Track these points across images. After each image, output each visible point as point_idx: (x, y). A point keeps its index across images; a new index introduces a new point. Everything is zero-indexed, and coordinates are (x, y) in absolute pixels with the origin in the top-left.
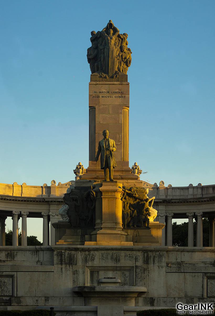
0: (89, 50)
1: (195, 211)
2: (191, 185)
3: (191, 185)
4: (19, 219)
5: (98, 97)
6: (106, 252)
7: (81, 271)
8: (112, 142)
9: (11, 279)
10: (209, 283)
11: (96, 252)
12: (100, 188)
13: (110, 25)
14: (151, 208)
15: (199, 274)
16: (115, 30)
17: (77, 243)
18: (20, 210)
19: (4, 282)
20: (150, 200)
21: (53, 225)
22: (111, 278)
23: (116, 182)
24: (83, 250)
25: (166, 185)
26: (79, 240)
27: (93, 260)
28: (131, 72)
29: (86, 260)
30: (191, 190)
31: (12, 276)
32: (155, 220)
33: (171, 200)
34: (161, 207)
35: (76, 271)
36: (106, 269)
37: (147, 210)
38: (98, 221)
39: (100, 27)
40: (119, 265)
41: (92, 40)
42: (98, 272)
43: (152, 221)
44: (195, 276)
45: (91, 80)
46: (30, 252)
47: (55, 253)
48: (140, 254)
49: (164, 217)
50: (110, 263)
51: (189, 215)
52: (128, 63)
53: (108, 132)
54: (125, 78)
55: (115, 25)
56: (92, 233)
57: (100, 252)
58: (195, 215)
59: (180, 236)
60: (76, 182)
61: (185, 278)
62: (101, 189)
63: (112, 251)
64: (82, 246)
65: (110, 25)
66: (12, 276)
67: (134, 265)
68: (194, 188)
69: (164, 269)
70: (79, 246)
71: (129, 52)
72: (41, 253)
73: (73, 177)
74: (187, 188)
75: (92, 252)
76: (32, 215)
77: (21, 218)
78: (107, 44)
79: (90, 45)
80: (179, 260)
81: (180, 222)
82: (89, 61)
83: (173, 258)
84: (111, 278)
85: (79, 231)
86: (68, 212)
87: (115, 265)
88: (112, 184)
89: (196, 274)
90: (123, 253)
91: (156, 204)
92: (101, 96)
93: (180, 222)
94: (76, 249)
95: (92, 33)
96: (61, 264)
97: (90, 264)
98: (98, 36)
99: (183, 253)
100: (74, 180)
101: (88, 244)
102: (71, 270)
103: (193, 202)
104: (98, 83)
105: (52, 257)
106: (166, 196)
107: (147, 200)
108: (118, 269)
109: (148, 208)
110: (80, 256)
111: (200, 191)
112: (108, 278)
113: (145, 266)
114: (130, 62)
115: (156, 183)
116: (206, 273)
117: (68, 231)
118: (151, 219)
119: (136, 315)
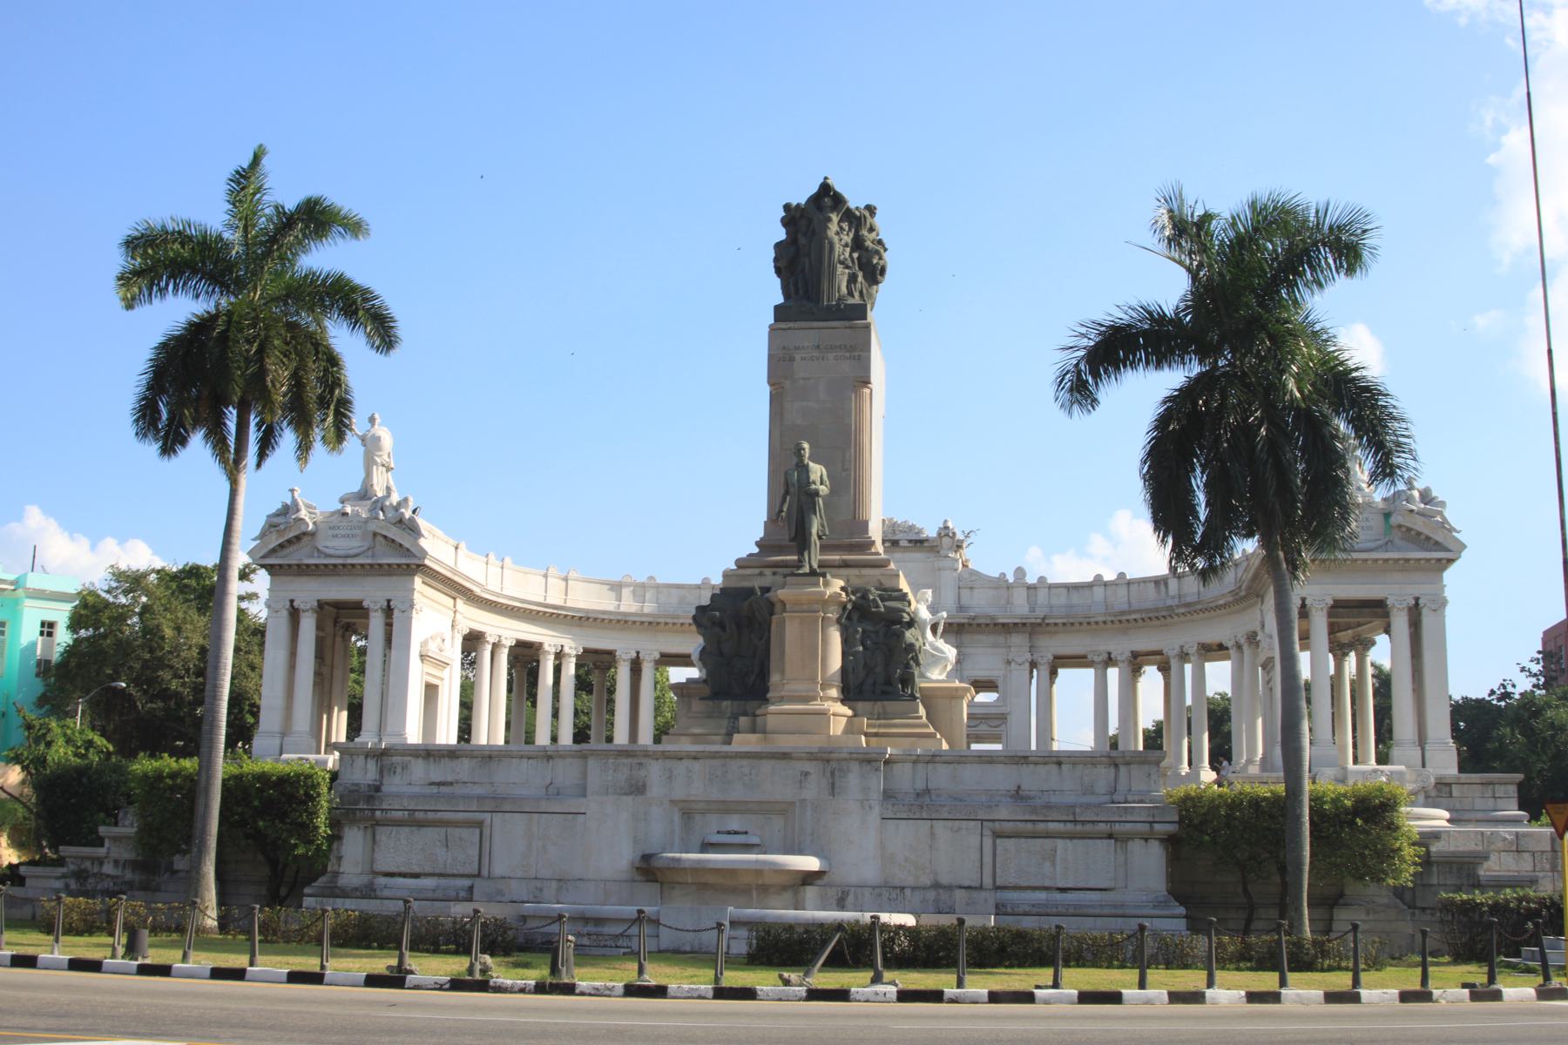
2: (1098, 578)
3: (1098, 578)
5: (792, 359)
8: (817, 471)
10: (999, 849)
13: (825, 188)
15: (972, 823)
16: (838, 200)
18: (388, 595)
22: (736, 833)
25: (1031, 579)
30: (1099, 592)
31: (479, 825)
38: (775, 678)
39: (801, 195)
51: (1096, 659)
52: (873, 272)
53: (806, 446)
55: (839, 186)
56: (758, 712)
61: (932, 835)
64: (726, 748)
65: (825, 188)
66: (479, 825)
68: (1106, 584)
69: (877, 810)
71: (879, 248)
74: (1089, 586)
79: (781, 234)
82: (778, 271)
84: (736, 833)
85: (726, 704)
92: (798, 357)
95: (787, 207)
101: (744, 742)
104: (791, 325)
106: (1032, 610)
111: (1122, 591)
112: (729, 833)
119: (6, 863)
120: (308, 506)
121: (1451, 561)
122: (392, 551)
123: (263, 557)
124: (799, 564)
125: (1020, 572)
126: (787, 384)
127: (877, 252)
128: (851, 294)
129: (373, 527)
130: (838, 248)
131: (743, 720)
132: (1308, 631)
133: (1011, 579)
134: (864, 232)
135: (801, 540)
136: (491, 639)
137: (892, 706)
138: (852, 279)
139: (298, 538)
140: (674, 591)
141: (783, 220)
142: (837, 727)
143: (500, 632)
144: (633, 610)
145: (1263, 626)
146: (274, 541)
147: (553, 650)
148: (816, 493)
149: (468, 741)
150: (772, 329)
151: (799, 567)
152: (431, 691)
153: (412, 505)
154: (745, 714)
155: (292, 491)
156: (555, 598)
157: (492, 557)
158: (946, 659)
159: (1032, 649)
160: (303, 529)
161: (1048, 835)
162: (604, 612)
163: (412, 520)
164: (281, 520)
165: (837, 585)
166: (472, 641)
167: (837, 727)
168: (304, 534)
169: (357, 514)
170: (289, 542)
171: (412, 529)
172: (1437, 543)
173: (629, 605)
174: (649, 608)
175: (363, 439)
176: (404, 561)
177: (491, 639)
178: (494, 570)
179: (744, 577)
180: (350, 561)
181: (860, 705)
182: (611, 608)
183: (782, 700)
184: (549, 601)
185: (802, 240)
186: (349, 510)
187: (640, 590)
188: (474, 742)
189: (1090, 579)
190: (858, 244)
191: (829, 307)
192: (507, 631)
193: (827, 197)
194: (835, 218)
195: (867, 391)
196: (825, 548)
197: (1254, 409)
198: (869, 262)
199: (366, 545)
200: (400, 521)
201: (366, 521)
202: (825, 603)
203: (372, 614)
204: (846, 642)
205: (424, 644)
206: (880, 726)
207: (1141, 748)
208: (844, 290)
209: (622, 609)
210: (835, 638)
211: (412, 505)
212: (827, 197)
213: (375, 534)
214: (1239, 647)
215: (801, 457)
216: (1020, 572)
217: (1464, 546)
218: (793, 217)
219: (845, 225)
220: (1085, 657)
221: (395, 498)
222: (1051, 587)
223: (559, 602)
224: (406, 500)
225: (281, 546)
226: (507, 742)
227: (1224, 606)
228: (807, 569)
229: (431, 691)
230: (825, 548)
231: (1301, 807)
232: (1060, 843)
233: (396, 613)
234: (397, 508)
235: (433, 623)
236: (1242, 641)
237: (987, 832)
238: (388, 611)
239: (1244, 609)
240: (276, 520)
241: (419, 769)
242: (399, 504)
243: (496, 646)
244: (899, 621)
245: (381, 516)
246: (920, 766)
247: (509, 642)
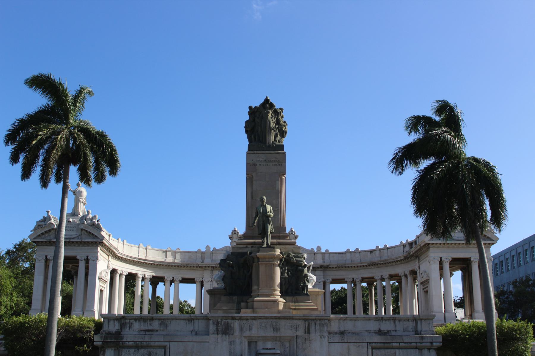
0: (246, 122)
1: (354, 276)
2: (348, 250)
3: (348, 250)
4: (171, 284)
5: (256, 165)
6: (265, 321)
7: (238, 341)
8: (269, 208)
9: (163, 350)
11: (254, 321)
12: (257, 254)
13: (267, 101)
14: (310, 274)
15: (364, 344)
16: (272, 106)
17: (232, 311)
18: (87, 254)
19: (156, 353)
20: (308, 265)
21: (209, 292)
22: (270, 349)
23: (274, 248)
24: (241, 319)
25: (323, 250)
26: (235, 308)
27: (250, 329)
28: (285, 141)
29: (242, 330)
31: (165, 347)
32: (314, 287)
33: (331, 266)
34: (319, 273)
35: (233, 342)
36: (265, 339)
37: (306, 276)
38: (255, 288)
39: (257, 102)
40: (278, 334)
41: (250, 114)
42: (256, 342)
43: (311, 287)
44: (359, 346)
45: (249, 149)
46: (184, 321)
47: (211, 322)
48: (300, 323)
49: (322, 283)
50: (270, 333)
51: (348, 280)
52: (283, 134)
53: (265, 198)
54: (282, 147)
55: (271, 100)
57: (259, 321)
58: (353, 280)
59: (339, 303)
60: (233, 248)
61: (349, 349)
62: (258, 254)
63: (271, 320)
65: (267, 101)
67: (295, 335)
68: (351, 253)
69: (326, 339)
70: (236, 315)
71: (285, 124)
72: (196, 322)
73: (227, 243)
75: (250, 321)
76: (185, 281)
77: (173, 284)
78: (266, 122)
79: (247, 118)
80: (342, 329)
81: (337, 287)
82: (247, 132)
83: (335, 326)
84: (270, 349)
85: (235, 298)
86: (224, 279)
87: (275, 335)
88: (270, 249)
89: (360, 344)
90: (283, 322)
91: (315, 270)
92: (258, 164)
93: (337, 287)
94: (233, 318)
95: (250, 108)
96: (218, 334)
97: (247, 333)
98: (256, 110)
99: (345, 322)
100: (229, 245)
101: (245, 313)
102: (227, 340)
103: (351, 267)
104: (255, 152)
105: (208, 326)
106: (324, 262)
107: (305, 266)
108: (278, 339)
109: (306, 275)
110: (236, 325)
112: (267, 349)
113: (306, 336)
114: (286, 133)
115: (313, 249)
116: (370, 343)
117: (223, 298)
118: (310, 286)
120: (54, 218)
121: (493, 244)
122: (89, 237)
123: (35, 238)
124: (262, 243)
125: (319, 248)
126: (254, 174)
127: (284, 126)
128: (275, 140)
129: (82, 227)
130: (272, 124)
131: (243, 304)
132: (440, 270)
133: (315, 250)
134: (280, 118)
135: (264, 233)
136: (119, 272)
137: (299, 298)
138: (276, 135)
139: (50, 231)
140: (187, 254)
141: (249, 112)
142: (281, 307)
143: (123, 269)
144: (171, 261)
145: (419, 268)
146: (40, 232)
147: (141, 277)
148: (270, 216)
149: (399, 313)
150: (247, 153)
151: (263, 245)
152: (101, 291)
153: (97, 218)
154: (243, 302)
155: (48, 212)
156: (142, 256)
157: (120, 239)
158: (313, 280)
159: (324, 277)
160: (52, 227)
161: (393, 348)
162: (161, 262)
163: (98, 224)
164: (43, 223)
165: (278, 252)
166: (113, 272)
167: (281, 307)
168: (53, 229)
169: (75, 222)
170: (46, 232)
171: (99, 228)
172: (488, 238)
173: (170, 259)
174: (178, 260)
175: (74, 193)
176: (94, 241)
177: (119, 272)
178: (121, 245)
179: (240, 248)
180: (72, 240)
181: (287, 298)
182: (163, 260)
183: (258, 296)
184: (140, 257)
185: (257, 120)
186: (71, 220)
187: (174, 253)
188: (164, 313)
189: (344, 250)
190: (278, 122)
191: (269, 146)
192: (125, 269)
193: (267, 104)
194: (271, 112)
195: (284, 177)
196: (273, 237)
197: (453, 188)
198: (282, 128)
199: (78, 234)
200: (93, 225)
201: (78, 225)
202: (274, 258)
203: (80, 262)
204: (282, 273)
205: (101, 273)
206: (296, 306)
207: (392, 313)
208: (273, 140)
209: (167, 261)
210: (278, 270)
211: (97, 218)
212: (267, 104)
213: (82, 230)
214: (406, 276)
215: (263, 202)
216: (319, 248)
217: (498, 239)
218: (253, 111)
219: (273, 115)
220: (344, 279)
221: (91, 216)
222: (330, 253)
223: (144, 258)
224: (95, 216)
225: (42, 234)
226: (149, 312)
227: (401, 260)
228: (265, 245)
229: (101, 291)
230: (273, 237)
231: (494, 336)
232: (397, 350)
233: (90, 261)
234: (91, 220)
235: (103, 264)
236: (407, 274)
237: (370, 347)
238: (87, 261)
239: (408, 262)
240: (41, 223)
241: (136, 326)
242: (93, 218)
243: (121, 275)
244: (301, 266)
245: (86, 223)
246: (341, 321)
247: (125, 274)
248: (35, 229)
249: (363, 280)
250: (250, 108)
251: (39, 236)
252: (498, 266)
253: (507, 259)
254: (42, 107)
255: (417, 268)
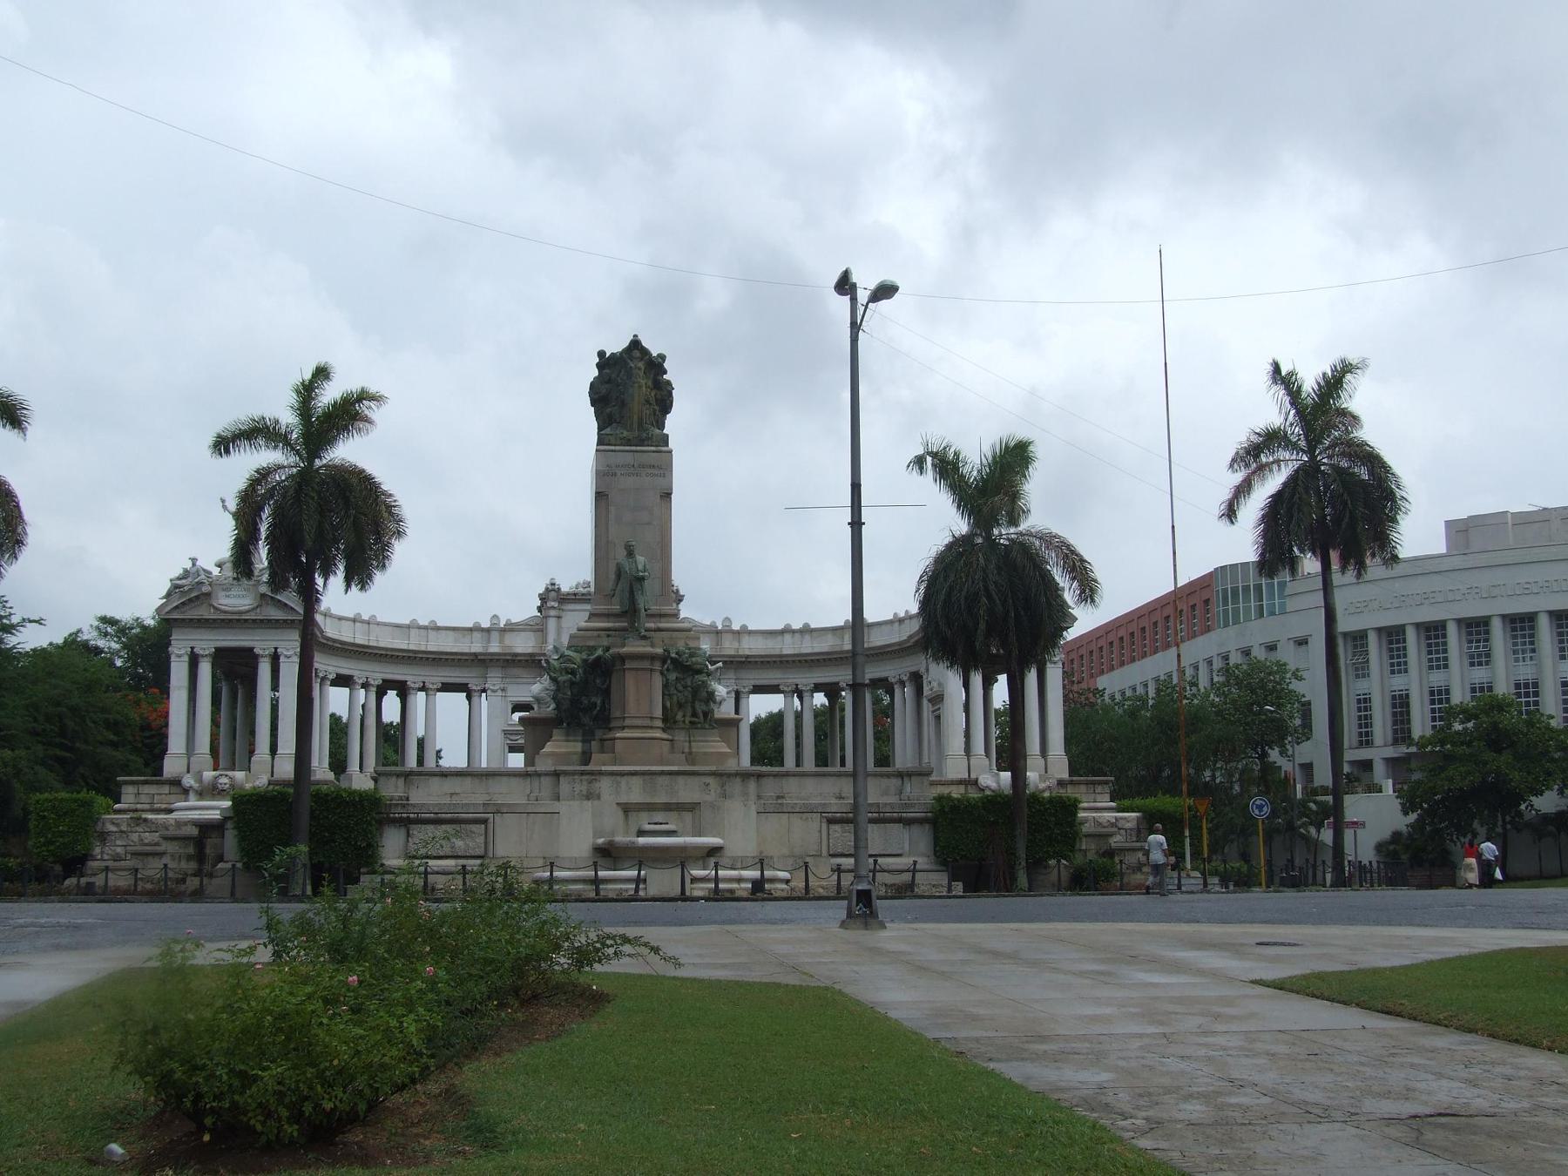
18: (275, 644)
31: (485, 821)
76: (447, 688)
95: (601, 354)
179: (589, 638)
214: (902, 684)
218: (606, 363)
233: (282, 659)
248: (168, 595)
249: (818, 688)
250: (601, 354)
251: (177, 607)
252: (1159, 629)
253: (1155, 624)
254: (485, 531)
255: (923, 670)
